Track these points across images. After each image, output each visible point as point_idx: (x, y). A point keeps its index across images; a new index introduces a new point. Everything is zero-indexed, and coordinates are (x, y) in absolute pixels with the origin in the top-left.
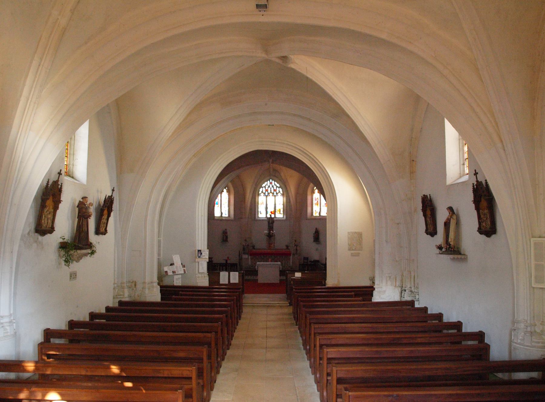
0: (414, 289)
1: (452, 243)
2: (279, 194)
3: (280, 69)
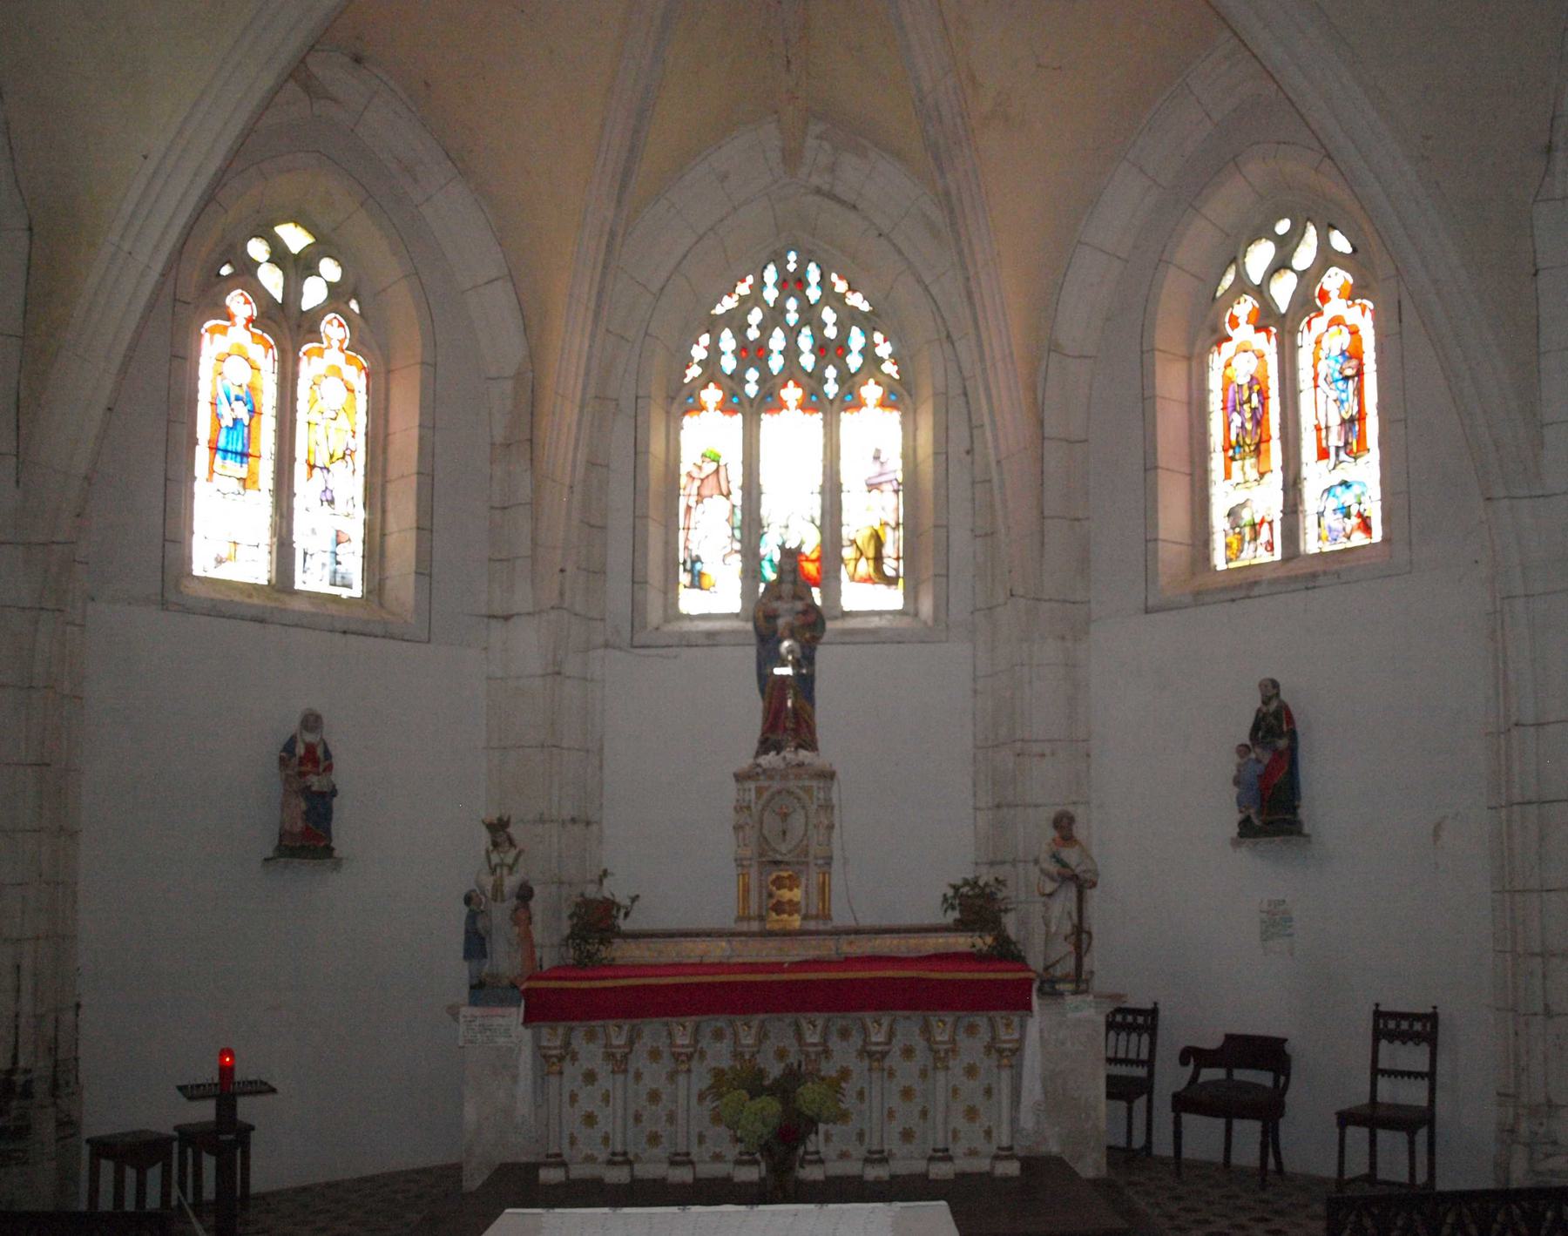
2: (871, 392)
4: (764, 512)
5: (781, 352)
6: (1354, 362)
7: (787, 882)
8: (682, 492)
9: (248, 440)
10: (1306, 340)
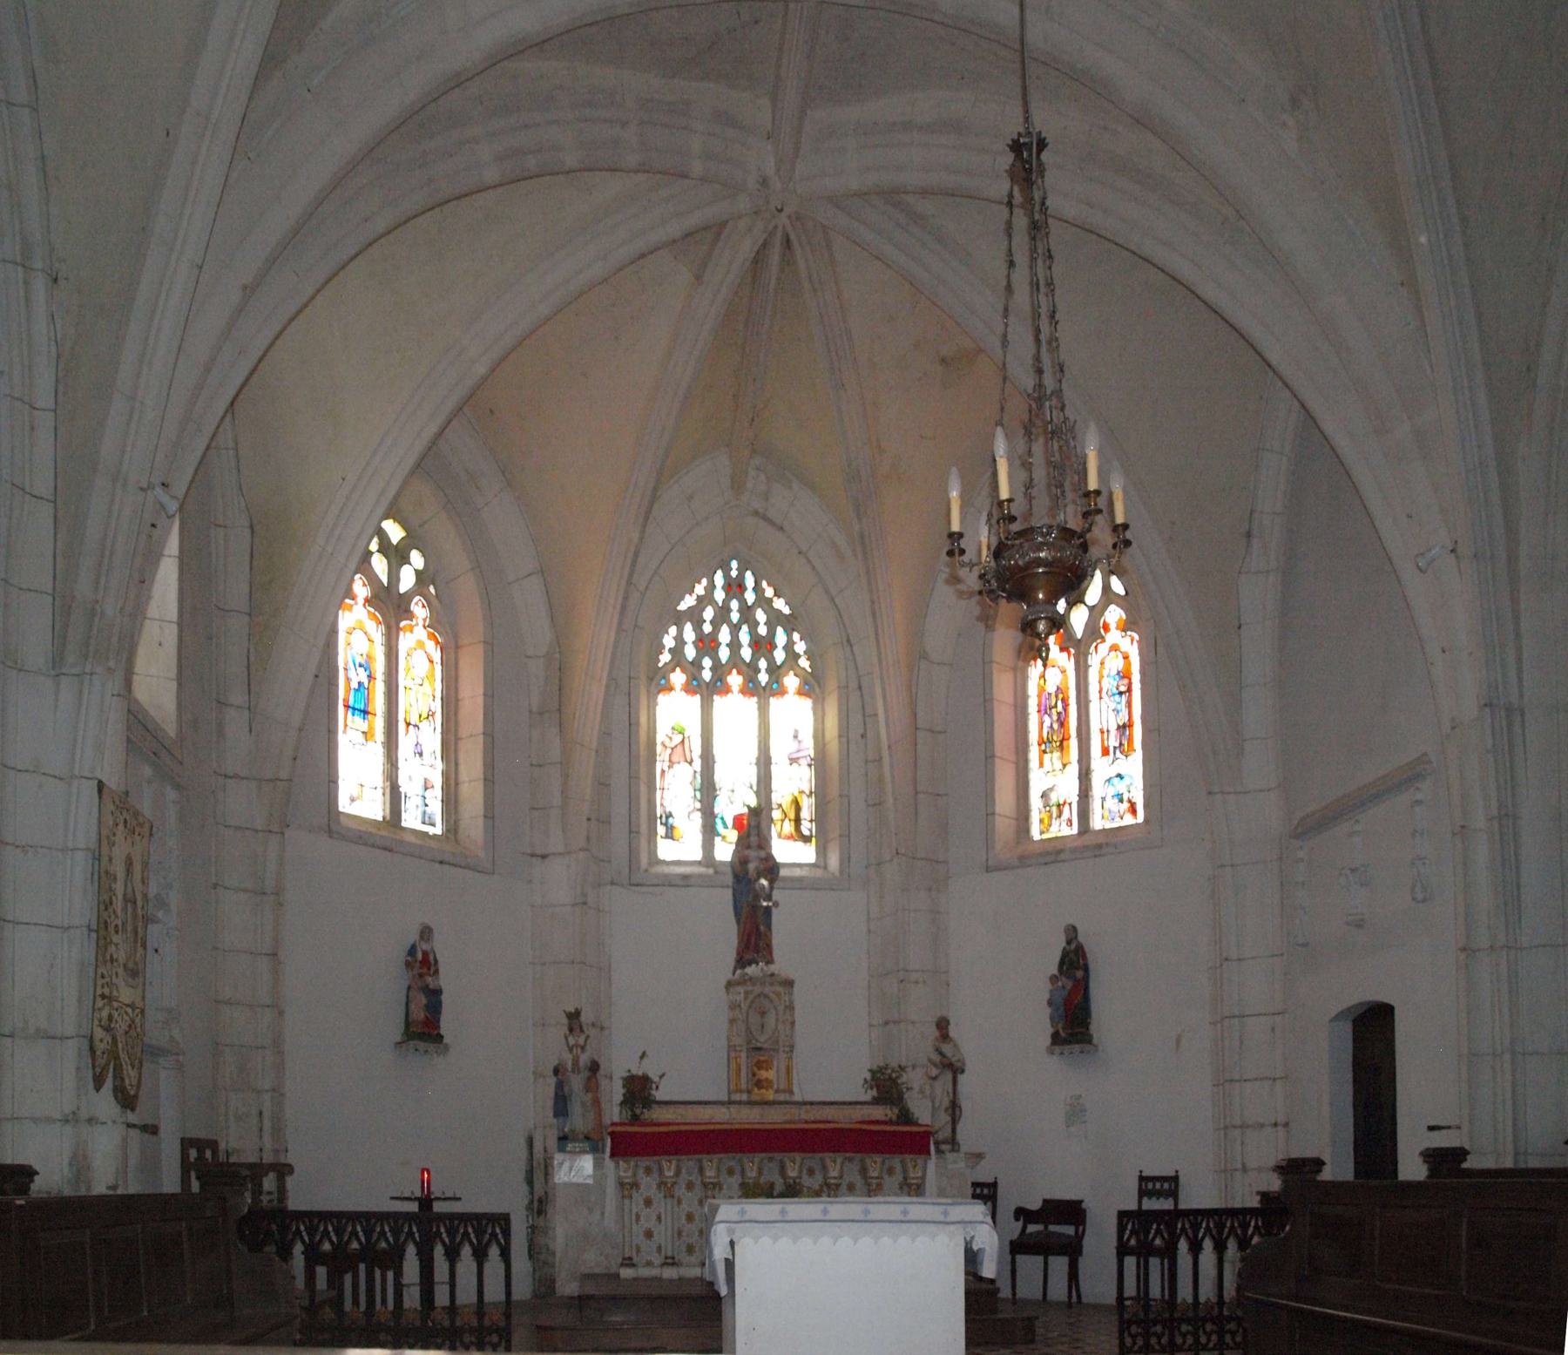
2: (791, 681)
4: (717, 778)
5: (727, 645)
6: (1126, 681)
7: (764, 1065)
8: (658, 758)
9: (368, 700)
10: (1094, 660)
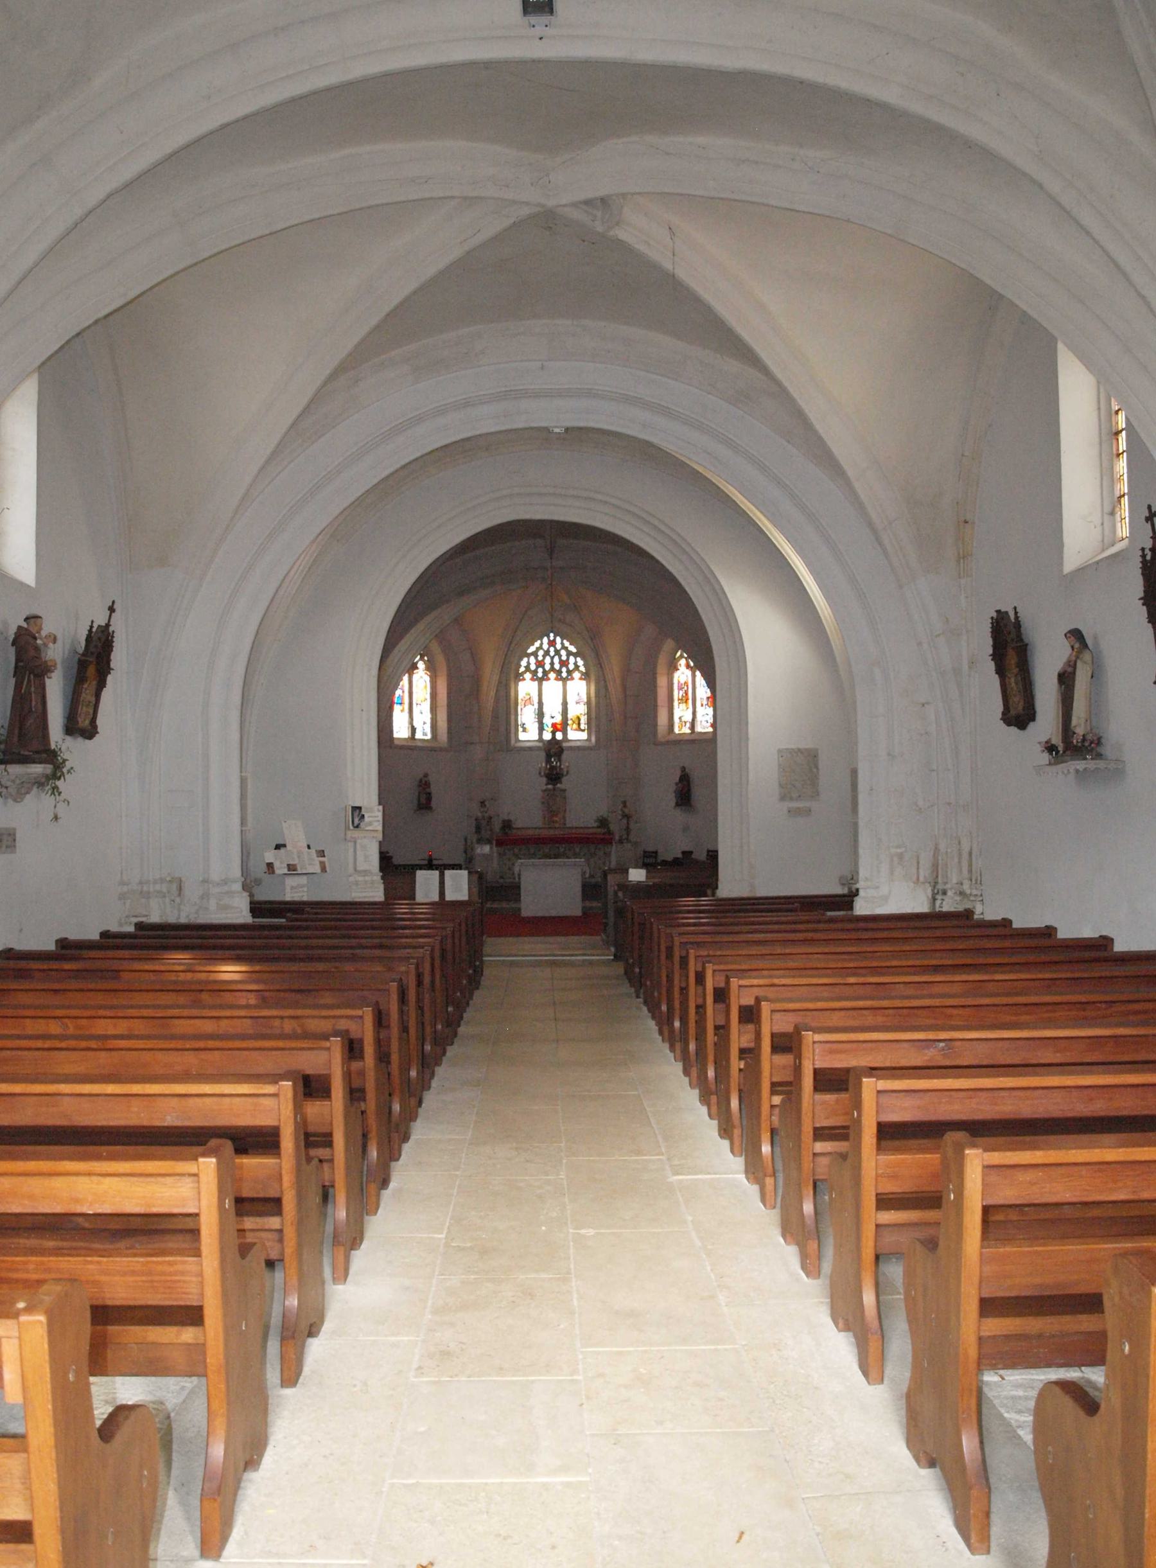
0: (971, 889)
1: (1080, 731)
2: (577, 675)
3: (584, 241)
